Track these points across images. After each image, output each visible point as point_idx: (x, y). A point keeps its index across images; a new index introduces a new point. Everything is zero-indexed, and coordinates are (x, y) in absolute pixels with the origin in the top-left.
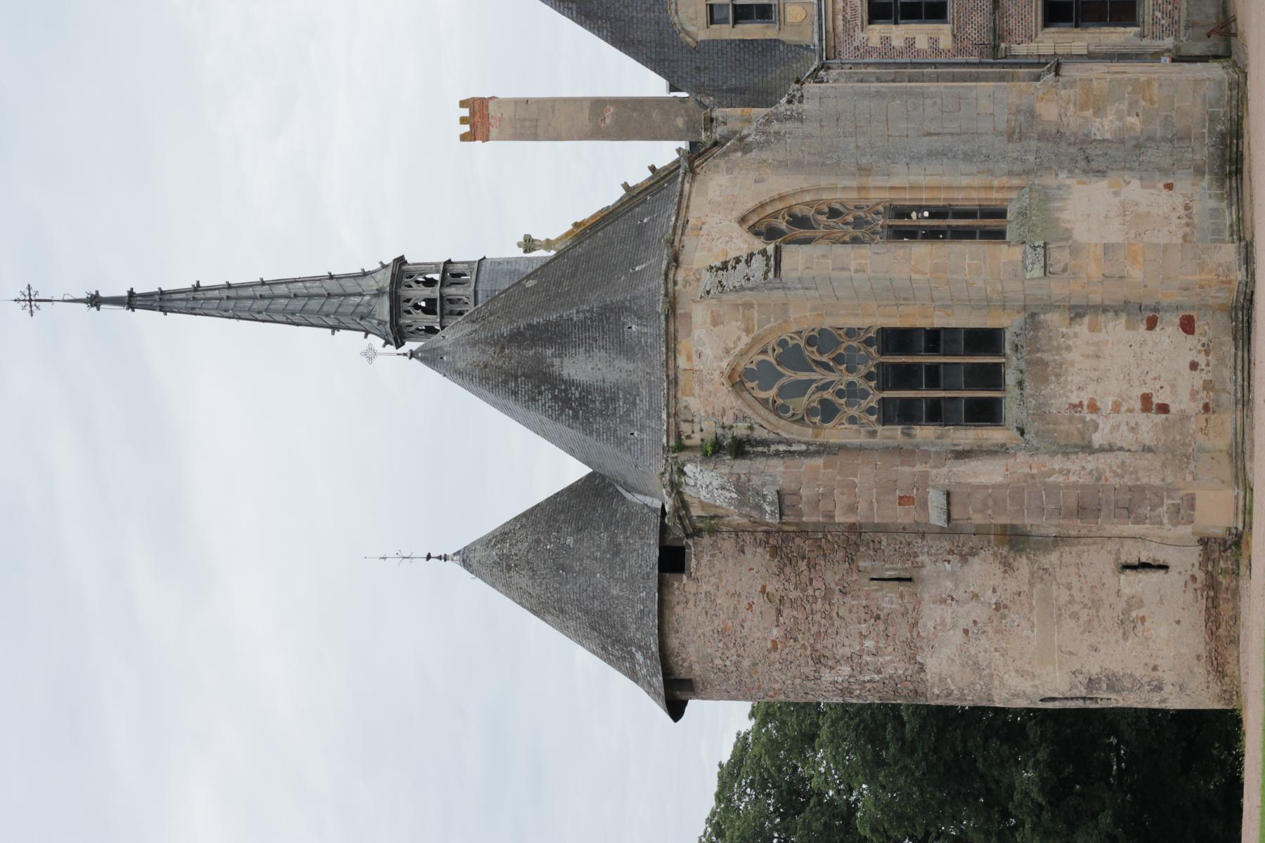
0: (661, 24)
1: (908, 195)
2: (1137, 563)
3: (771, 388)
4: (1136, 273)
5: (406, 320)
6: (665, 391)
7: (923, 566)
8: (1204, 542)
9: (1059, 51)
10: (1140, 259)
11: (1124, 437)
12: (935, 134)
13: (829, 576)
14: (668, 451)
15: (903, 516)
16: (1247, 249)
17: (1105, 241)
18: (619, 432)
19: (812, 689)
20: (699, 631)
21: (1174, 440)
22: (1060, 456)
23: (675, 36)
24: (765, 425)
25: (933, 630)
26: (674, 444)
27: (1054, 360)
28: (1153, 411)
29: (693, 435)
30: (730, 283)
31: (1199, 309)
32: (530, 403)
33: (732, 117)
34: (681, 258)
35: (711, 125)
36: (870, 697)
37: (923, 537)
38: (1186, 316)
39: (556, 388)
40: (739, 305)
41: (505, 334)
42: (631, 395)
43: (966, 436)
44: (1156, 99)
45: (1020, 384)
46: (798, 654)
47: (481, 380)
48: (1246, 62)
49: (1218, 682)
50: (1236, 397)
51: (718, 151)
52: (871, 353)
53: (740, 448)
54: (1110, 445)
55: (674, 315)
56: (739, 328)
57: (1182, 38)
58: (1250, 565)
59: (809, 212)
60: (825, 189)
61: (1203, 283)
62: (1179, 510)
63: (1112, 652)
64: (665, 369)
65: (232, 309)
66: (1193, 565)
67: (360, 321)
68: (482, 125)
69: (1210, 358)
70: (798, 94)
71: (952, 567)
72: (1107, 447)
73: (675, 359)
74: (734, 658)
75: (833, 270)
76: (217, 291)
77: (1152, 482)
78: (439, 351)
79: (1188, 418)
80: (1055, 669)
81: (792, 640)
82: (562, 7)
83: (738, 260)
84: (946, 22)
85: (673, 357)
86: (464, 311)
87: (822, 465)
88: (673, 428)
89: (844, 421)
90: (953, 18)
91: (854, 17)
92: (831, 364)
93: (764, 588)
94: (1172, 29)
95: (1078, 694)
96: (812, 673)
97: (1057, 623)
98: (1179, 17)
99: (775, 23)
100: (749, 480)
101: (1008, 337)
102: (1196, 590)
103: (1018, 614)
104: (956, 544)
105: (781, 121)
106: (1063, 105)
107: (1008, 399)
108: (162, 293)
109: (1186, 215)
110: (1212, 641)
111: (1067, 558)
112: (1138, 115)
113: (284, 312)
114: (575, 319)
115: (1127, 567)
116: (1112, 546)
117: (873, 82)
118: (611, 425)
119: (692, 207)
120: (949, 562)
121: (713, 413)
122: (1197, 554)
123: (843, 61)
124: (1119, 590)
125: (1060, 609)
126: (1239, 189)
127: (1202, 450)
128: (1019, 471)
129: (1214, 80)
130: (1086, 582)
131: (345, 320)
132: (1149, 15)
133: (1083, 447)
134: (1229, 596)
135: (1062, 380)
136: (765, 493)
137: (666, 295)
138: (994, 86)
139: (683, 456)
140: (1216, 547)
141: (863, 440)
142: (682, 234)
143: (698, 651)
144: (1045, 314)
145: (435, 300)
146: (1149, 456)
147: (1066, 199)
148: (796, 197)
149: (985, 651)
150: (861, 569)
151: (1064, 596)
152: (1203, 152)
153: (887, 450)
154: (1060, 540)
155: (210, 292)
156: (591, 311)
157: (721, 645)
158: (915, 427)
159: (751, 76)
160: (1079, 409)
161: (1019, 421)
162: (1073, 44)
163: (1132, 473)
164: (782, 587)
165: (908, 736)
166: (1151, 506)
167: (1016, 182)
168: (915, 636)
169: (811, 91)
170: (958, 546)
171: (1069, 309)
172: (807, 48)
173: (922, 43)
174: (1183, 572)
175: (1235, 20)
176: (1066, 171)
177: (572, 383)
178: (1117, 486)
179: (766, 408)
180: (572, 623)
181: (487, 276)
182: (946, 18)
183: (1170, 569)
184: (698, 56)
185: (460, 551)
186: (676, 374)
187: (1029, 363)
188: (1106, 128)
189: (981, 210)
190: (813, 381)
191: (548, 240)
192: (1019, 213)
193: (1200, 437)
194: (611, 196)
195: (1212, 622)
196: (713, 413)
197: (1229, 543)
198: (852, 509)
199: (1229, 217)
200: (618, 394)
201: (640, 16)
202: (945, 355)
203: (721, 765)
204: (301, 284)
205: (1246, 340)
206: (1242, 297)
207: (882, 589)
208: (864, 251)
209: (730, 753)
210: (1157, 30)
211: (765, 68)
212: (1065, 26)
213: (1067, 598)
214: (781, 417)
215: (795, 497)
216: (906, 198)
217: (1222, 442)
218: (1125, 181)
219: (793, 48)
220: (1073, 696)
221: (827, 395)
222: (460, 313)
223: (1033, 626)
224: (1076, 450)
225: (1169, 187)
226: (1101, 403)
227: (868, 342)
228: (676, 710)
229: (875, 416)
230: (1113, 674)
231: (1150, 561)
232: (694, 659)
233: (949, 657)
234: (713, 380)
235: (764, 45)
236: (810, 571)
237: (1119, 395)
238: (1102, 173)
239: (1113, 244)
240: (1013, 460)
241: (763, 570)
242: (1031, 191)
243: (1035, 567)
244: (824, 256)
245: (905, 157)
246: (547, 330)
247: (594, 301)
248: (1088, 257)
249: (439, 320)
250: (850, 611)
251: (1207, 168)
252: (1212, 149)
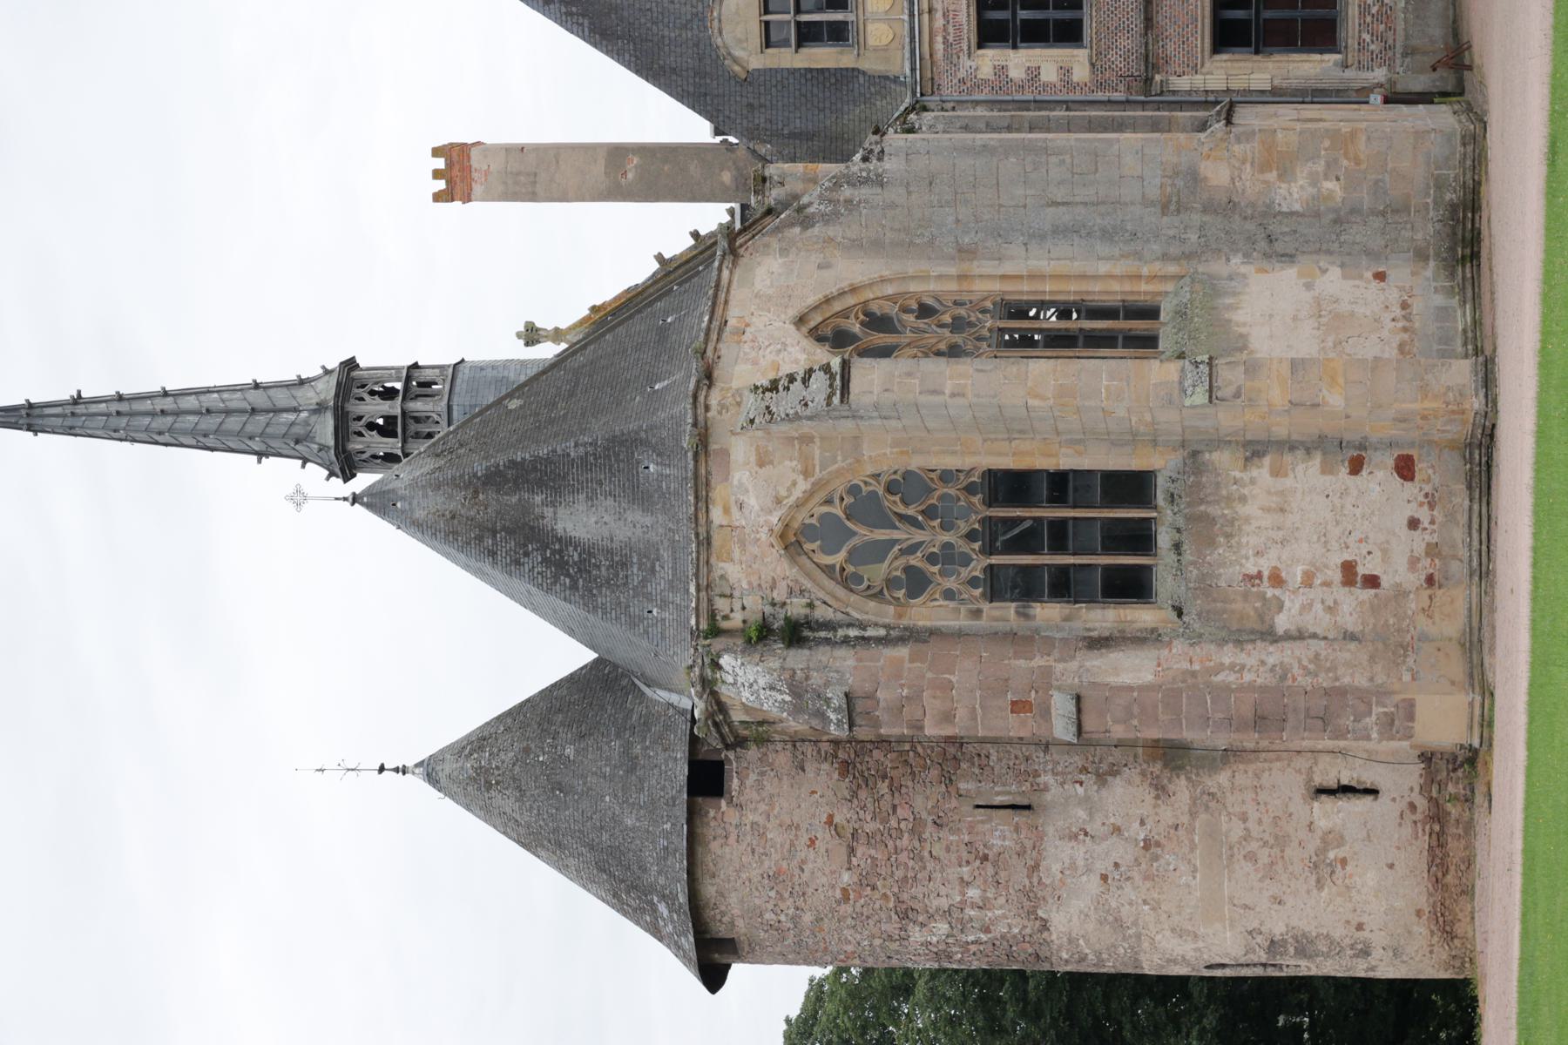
0: (702, 46)
1: (1025, 287)
2: (1335, 786)
3: (838, 551)
4: (1335, 399)
5: (355, 445)
6: (694, 555)
7: (1046, 789)
8: (1427, 757)
9: (1234, 86)
10: (1341, 380)
11: (1318, 620)
12: (1064, 204)
13: (919, 802)
14: (698, 637)
15: (1015, 726)
16: (1486, 368)
17: (1293, 354)
18: (632, 609)
19: (897, 952)
20: (744, 876)
21: (1386, 624)
22: (1231, 645)
23: (719, 62)
24: (830, 601)
26: (706, 627)
27: (1224, 516)
28: (1358, 585)
29: (732, 615)
30: (781, 409)
31: (1421, 447)
32: (513, 568)
33: (789, 174)
34: (716, 374)
35: (763, 186)
36: (975, 963)
38: (1403, 456)
39: (548, 547)
40: (793, 438)
41: (479, 474)
42: (649, 557)
43: (1104, 617)
44: (1362, 157)
45: (1177, 547)
46: (877, 906)
47: (447, 535)
48: (1485, 107)
49: (1445, 945)
50: (1470, 566)
51: (772, 223)
52: (974, 504)
53: (796, 634)
54: (1299, 631)
55: (706, 452)
56: (794, 471)
57: (1397, 70)
58: (1490, 795)
59: (892, 310)
60: (913, 278)
61: (1426, 413)
63: (1303, 906)
64: (693, 526)
65: (124, 429)
66: (1412, 789)
67: (296, 445)
68: (462, 181)
69: (1435, 513)
70: (877, 149)
71: (1086, 791)
72: (1295, 633)
73: (707, 512)
74: (791, 911)
75: (920, 393)
76: (104, 405)
77: (1356, 683)
78: (391, 495)
79: (1406, 594)
80: (1225, 928)
81: (869, 888)
82: (570, 22)
83: (792, 378)
84: (1082, 47)
85: (704, 509)
86: (434, 433)
87: (907, 658)
88: (704, 605)
89: (937, 596)
90: (1091, 41)
91: (959, 39)
92: (920, 518)
93: (831, 817)
94: (1385, 56)
95: (1256, 960)
96: (897, 932)
97: (1228, 866)
98: (1394, 40)
99: (853, 46)
100: (807, 678)
101: (1161, 482)
102: (1415, 822)
103: (1174, 854)
105: (854, 185)
106: (1237, 165)
107: (1160, 568)
108: (30, 406)
109: (1404, 316)
110: (1436, 891)
111: (1241, 779)
112: (1338, 179)
113: (193, 432)
114: (572, 454)
115: (1322, 791)
116: (1302, 763)
117: (981, 132)
118: (622, 599)
119: (732, 303)
120: (1081, 784)
121: (759, 585)
122: (1417, 775)
123: (944, 98)
124: (1312, 823)
125: (1231, 848)
126: (1475, 282)
127: (1424, 638)
128: (1175, 667)
129: (1441, 131)
130: (1267, 811)
131: (275, 444)
132: (1353, 38)
133: (1262, 633)
134: (1460, 831)
135: (1233, 541)
136: (830, 695)
137: (695, 425)
138: (1145, 139)
139: (718, 643)
140: (1442, 765)
141: (963, 622)
142: (718, 340)
143: (742, 901)
144: (1210, 452)
145: (396, 417)
146: (1353, 646)
147: (1239, 293)
148: (875, 288)
149: (1131, 904)
150: (962, 792)
151: (1237, 831)
152: (1427, 229)
153: (996, 637)
154: (1231, 755)
155: (94, 406)
156: (594, 444)
157: (773, 894)
158: (1033, 604)
159: (822, 116)
160: (1257, 581)
161: (1175, 597)
162: (1252, 76)
163: (1329, 670)
164: (855, 817)
165: (1032, 995)
166: (1355, 715)
167: (1172, 269)
168: (1036, 884)
169: (894, 144)
170: (1093, 762)
171: (1244, 446)
172: (896, 79)
173: (1049, 75)
174: (1398, 799)
175: (1470, 47)
176: (1240, 255)
177: (569, 542)
178: (1308, 689)
179: (832, 579)
180: (572, 862)
181: (464, 386)
182: (1082, 40)
183: (1380, 795)
184: (750, 89)
185: (423, 761)
186: (708, 532)
187: (1188, 519)
188: (1296, 196)
189: (1124, 307)
190: (895, 542)
191: (557, 330)
192: (1176, 313)
193: (1422, 622)
194: (642, 270)
195: (1437, 866)
196: (759, 585)
197: (1460, 759)
198: (948, 717)
199: (1462, 319)
200: (631, 557)
201: (673, 35)
202: (1075, 507)
203: (788, 1021)
204: (215, 395)
205: (1484, 489)
206: (1480, 431)
207: (990, 820)
208: (964, 366)
209: (800, 1006)
210: (1365, 58)
211: (839, 105)
212: (1242, 53)
213: (1241, 833)
214: (851, 590)
215: (869, 702)
216: (1023, 290)
217: (1452, 627)
218: (1320, 268)
219: (877, 80)
220: (1249, 962)
221: (915, 560)
222: (430, 436)
224: (1253, 637)
225: (1380, 276)
226: (1288, 573)
227: (970, 489)
228: (713, 978)
229: (980, 590)
230: (1304, 935)
231: (1354, 784)
232: (736, 912)
233: (1081, 912)
234: (759, 540)
235: (839, 75)
236: (893, 795)
237: (1312, 564)
238: (1289, 258)
239: (1303, 359)
240: (1166, 652)
242: (1193, 281)
243: (1199, 790)
244: (909, 374)
245: (1023, 235)
246: (535, 469)
247: (599, 429)
248: (1269, 377)
249: (400, 445)
250: (948, 850)
251: (1432, 252)
252: (1438, 226)
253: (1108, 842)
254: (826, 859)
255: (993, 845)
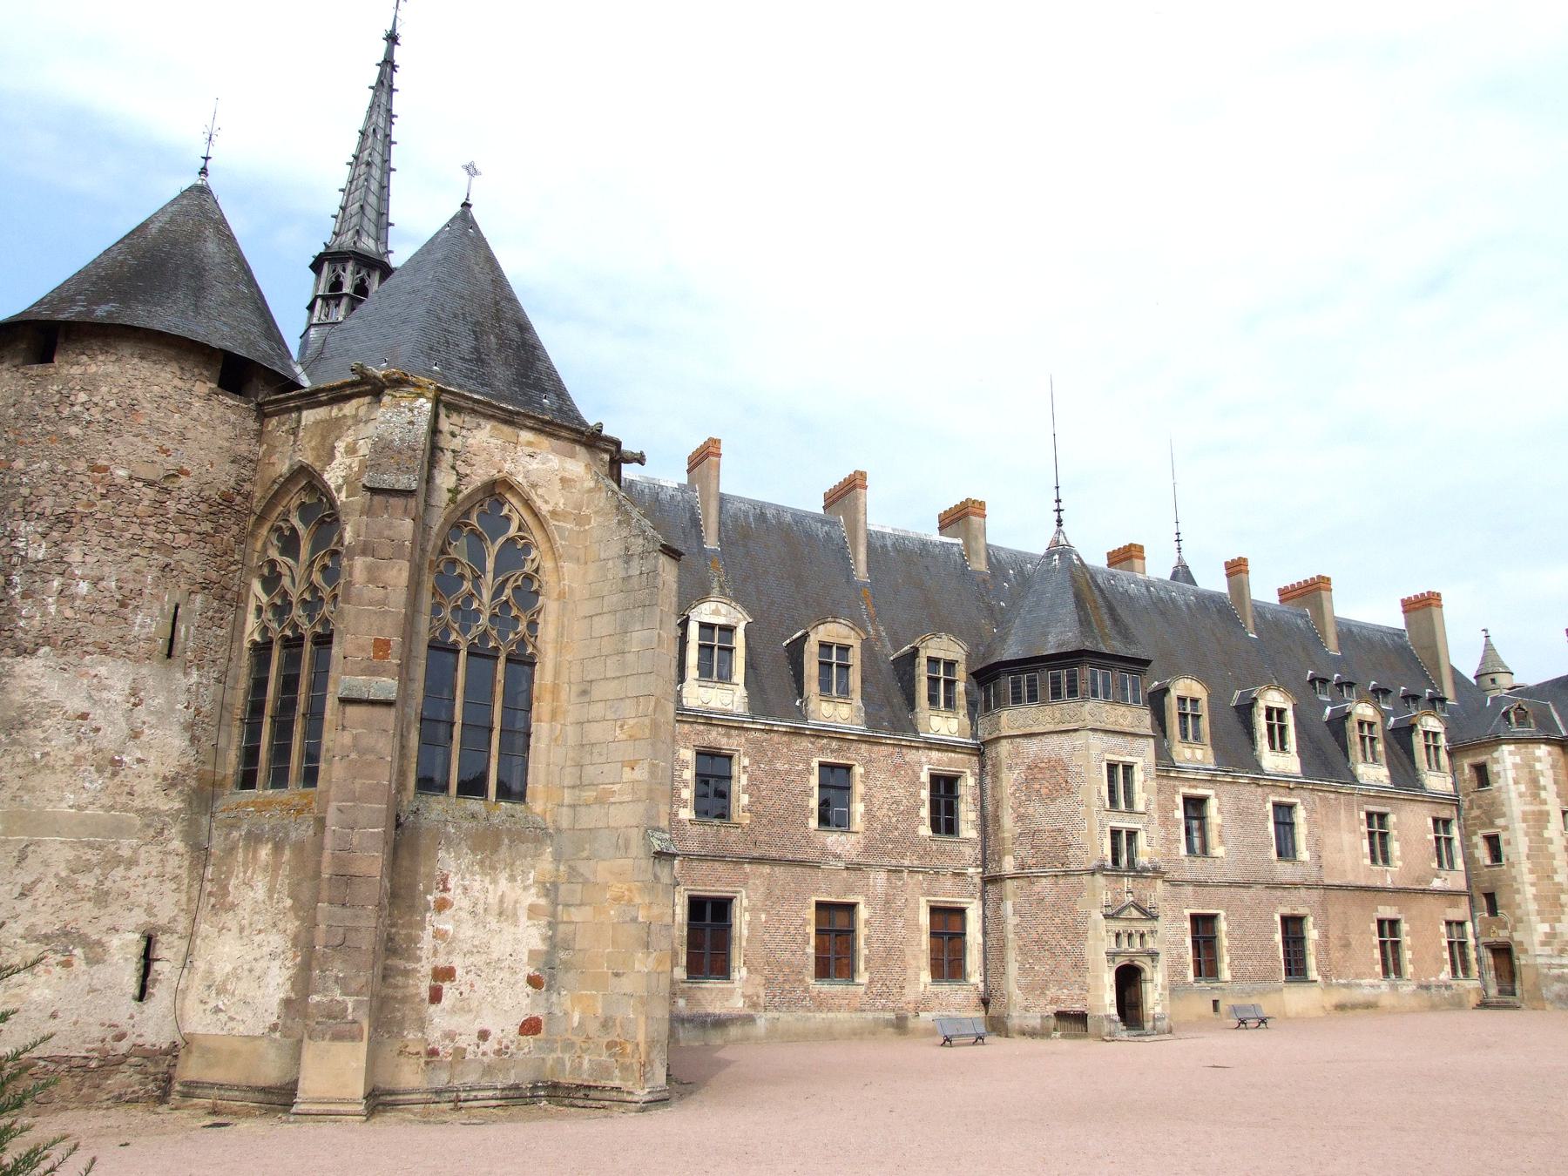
7: (186, 674)
13: (189, 555)
25: (94, 673)
37: (218, 681)
46: (79, 496)
62: (335, 1018)
74: (86, 416)
93: (187, 474)
104: (207, 720)
115: (149, 941)
116: (182, 925)
124: (117, 931)
157: (112, 404)
160: (441, 887)
166: (344, 978)
174: (132, 1022)
207: (163, 616)
223: (80, 808)
237: (454, 938)
241: (209, 479)
250: (136, 572)
253: (124, 724)
254: (145, 459)
255: (137, 615)
